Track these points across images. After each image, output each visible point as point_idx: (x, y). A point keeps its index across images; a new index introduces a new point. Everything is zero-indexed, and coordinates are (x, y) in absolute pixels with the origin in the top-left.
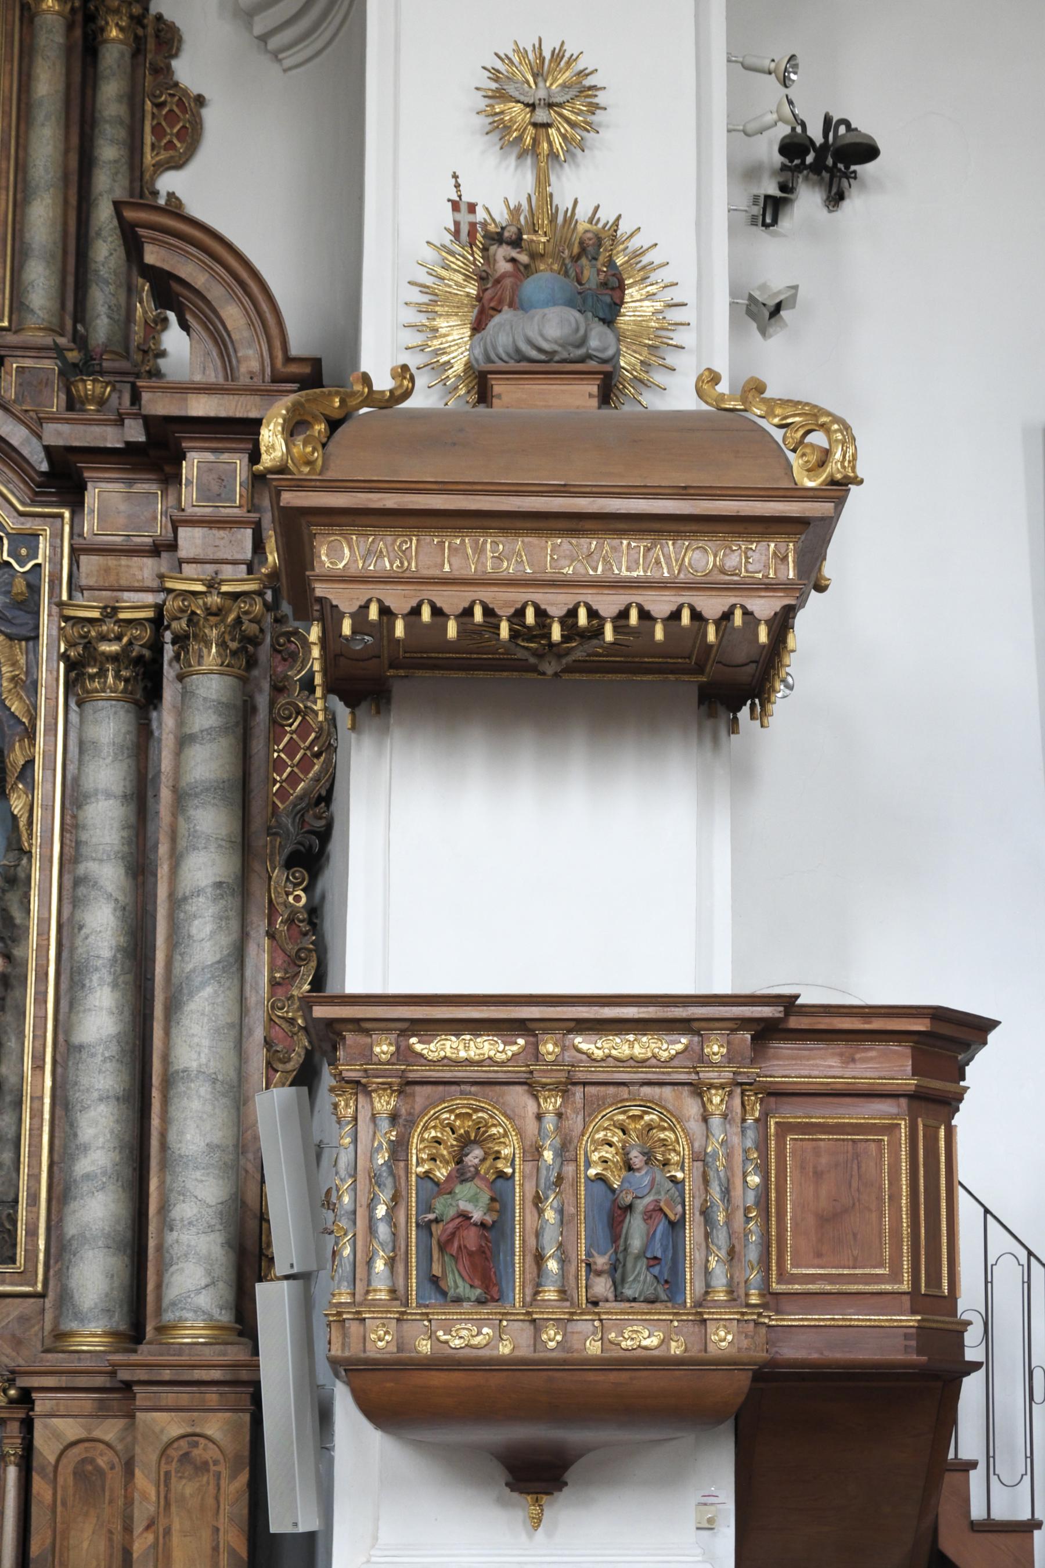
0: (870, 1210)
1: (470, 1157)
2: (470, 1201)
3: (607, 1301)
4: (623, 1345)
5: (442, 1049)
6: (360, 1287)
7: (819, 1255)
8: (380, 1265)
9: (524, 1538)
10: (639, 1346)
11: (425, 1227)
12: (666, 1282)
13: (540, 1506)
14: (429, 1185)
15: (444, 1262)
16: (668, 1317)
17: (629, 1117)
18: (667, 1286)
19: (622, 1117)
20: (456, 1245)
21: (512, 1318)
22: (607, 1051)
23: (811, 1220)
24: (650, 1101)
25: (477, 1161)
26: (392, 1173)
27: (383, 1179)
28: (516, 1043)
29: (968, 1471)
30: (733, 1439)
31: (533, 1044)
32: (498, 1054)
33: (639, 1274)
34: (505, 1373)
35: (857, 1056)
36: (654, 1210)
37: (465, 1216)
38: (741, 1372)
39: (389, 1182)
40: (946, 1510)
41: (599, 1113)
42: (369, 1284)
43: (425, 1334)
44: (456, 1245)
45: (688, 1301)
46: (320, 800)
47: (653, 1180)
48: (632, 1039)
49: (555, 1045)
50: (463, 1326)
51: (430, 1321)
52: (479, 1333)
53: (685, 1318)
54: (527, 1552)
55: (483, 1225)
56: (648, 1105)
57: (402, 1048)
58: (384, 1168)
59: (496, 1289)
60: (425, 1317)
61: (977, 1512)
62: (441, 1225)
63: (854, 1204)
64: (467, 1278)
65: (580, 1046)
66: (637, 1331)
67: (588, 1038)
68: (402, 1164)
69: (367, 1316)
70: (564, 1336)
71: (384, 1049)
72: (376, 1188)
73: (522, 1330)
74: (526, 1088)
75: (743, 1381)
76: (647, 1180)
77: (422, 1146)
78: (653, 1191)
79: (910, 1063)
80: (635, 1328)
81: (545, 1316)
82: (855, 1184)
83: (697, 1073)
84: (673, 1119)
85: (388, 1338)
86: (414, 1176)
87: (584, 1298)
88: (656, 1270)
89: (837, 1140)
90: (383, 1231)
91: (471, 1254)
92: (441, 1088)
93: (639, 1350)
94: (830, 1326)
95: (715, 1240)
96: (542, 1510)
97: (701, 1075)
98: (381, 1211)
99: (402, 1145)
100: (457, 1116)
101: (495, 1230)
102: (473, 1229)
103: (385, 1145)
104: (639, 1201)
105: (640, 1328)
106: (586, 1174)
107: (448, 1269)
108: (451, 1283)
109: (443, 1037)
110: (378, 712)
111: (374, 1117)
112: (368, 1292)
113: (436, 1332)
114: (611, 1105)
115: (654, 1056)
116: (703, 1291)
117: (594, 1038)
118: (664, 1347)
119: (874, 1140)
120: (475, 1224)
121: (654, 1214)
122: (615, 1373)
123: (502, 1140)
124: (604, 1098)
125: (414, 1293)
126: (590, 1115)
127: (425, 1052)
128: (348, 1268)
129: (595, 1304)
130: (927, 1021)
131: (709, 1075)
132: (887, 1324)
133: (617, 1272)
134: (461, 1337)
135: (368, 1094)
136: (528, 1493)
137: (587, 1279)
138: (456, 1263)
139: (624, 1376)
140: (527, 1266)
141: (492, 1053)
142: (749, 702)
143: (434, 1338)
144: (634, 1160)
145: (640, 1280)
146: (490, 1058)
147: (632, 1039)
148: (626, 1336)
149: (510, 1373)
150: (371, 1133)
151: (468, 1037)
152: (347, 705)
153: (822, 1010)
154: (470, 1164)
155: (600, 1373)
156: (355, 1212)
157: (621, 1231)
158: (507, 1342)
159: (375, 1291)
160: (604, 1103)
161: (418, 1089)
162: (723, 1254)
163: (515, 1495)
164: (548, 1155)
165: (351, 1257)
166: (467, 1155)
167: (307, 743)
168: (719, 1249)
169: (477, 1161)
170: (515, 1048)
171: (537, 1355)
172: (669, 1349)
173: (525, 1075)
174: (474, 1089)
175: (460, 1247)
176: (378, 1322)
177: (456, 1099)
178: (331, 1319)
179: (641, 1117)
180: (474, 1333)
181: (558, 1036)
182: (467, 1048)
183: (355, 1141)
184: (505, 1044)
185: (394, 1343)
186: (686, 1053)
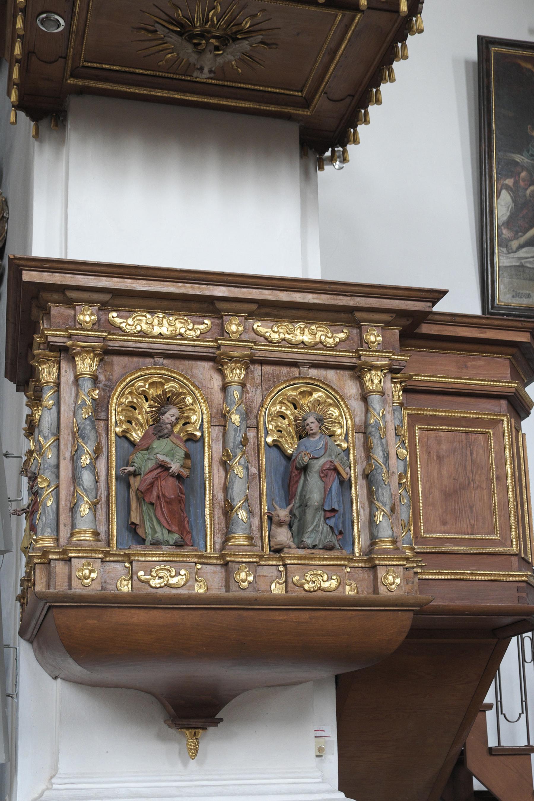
0: (482, 488)
1: (167, 415)
2: (166, 455)
3: (290, 547)
4: (306, 587)
5: (138, 324)
6: (64, 532)
7: (444, 523)
8: (84, 509)
9: (180, 766)
10: (319, 588)
11: (124, 480)
12: (341, 533)
13: (197, 739)
14: (126, 444)
15: (141, 511)
16: (342, 563)
17: (301, 393)
18: (340, 537)
19: (294, 393)
20: (155, 493)
21: (206, 561)
22: (282, 336)
23: (437, 494)
25: (173, 419)
26: (94, 428)
28: (204, 323)
29: (485, 711)
30: (335, 686)
31: (218, 325)
32: (188, 332)
33: (317, 525)
34: (200, 612)
35: (469, 364)
36: (329, 469)
37: (164, 467)
38: (404, 613)
39: (92, 435)
40: (471, 740)
41: (275, 388)
42: (73, 526)
43: (126, 575)
44: (155, 493)
45: (357, 550)
47: (326, 444)
48: (303, 326)
49: (238, 325)
50: (162, 567)
51: (131, 562)
52: (178, 574)
53: (356, 564)
54: (183, 778)
55: (179, 477)
56: (317, 384)
57: (102, 321)
58: (88, 422)
59: (189, 536)
60: (126, 559)
61: (492, 742)
62: (138, 478)
63: (469, 483)
64: (165, 524)
65: (259, 329)
66: (317, 574)
67: (265, 323)
68: (102, 423)
69: (73, 555)
70: (255, 577)
71: (87, 316)
72: (80, 441)
73: (215, 573)
74: (211, 364)
75: (406, 620)
76: (321, 444)
77: (119, 409)
78: (327, 453)
79: (509, 371)
80: (315, 572)
81: (240, 559)
82: (469, 467)
83: (359, 357)
84: (337, 398)
85: (94, 575)
86: (113, 435)
87: (268, 547)
88: (332, 522)
90: (87, 477)
91: (169, 502)
92: (136, 359)
93: (319, 591)
94: (460, 580)
95: (381, 498)
96: (198, 743)
97: (363, 358)
98: (85, 460)
99: (102, 407)
100: (152, 384)
101: (188, 482)
102: (171, 480)
103: (88, 403)
104: (315, 461)
105: (320, 572)
106: (266, 442)
107: (146, 517)
108: (149, 530)
109: (139, 313)
110: (56, 125)
111: (77, 379)
112: (72, 535)
113: (137, 572)
114: (285, 382)
116: (368, 543)
117: (270, 324)
118: (340, 589)
119: (481, 433)
120: (173, 476)
121: (330, 473)
122: (297, 613)
123: (191, 407)
124: (279, 376)
125: (115, 538)
126: (267, 390)
127: (123, 325)
128: (51, 516)
129: (278, 551)
130: (528, 334)
131: (367, 358)
132: (505, 579)
133: (297, 525)
134: (160, 578)
135: (72, 360)
136: (188, 728)
137: (269, 531)
138: (155, 510)
139: (306, 615)
140: (216, 518)
141: (183, 331)
142: (330, 149)
143: (135, 578)
144: (311, 425)
145: (317, 530)
146: (181, 334)
147: (303, 326)
148: (308, 579)
149: (204, 612)
150: (73, 395)
151: (161, 315)
152: (33, 119)
153: (449, 318)
154: (167, 421)
155: (285, 612)
156: (58, 467)
157: (296, 490)
158: (202, 583)
159: (80, 532)
160: (278, 380)
161: (116, 359)
162: (387, 509)
163: (173, 732)
164: (236, 418)
165: (54, 506)
166: (164, 414)
168: (384, 505)
169: (173, 419)
170: (202, 327)
171: (230, 595)
172: (344, 591)
173: (212, 350)
174: (166, 362)
175: (158, 496)
176: (84, 561)
177: (150, 369)
178: (36, 561)
179: (311, 394)
180: (173, 573)
181: (241, 318)
182: (161, 324)
183: (58, 404)
184: (194, 323)
185: (98, 581)
186: (347, 342)
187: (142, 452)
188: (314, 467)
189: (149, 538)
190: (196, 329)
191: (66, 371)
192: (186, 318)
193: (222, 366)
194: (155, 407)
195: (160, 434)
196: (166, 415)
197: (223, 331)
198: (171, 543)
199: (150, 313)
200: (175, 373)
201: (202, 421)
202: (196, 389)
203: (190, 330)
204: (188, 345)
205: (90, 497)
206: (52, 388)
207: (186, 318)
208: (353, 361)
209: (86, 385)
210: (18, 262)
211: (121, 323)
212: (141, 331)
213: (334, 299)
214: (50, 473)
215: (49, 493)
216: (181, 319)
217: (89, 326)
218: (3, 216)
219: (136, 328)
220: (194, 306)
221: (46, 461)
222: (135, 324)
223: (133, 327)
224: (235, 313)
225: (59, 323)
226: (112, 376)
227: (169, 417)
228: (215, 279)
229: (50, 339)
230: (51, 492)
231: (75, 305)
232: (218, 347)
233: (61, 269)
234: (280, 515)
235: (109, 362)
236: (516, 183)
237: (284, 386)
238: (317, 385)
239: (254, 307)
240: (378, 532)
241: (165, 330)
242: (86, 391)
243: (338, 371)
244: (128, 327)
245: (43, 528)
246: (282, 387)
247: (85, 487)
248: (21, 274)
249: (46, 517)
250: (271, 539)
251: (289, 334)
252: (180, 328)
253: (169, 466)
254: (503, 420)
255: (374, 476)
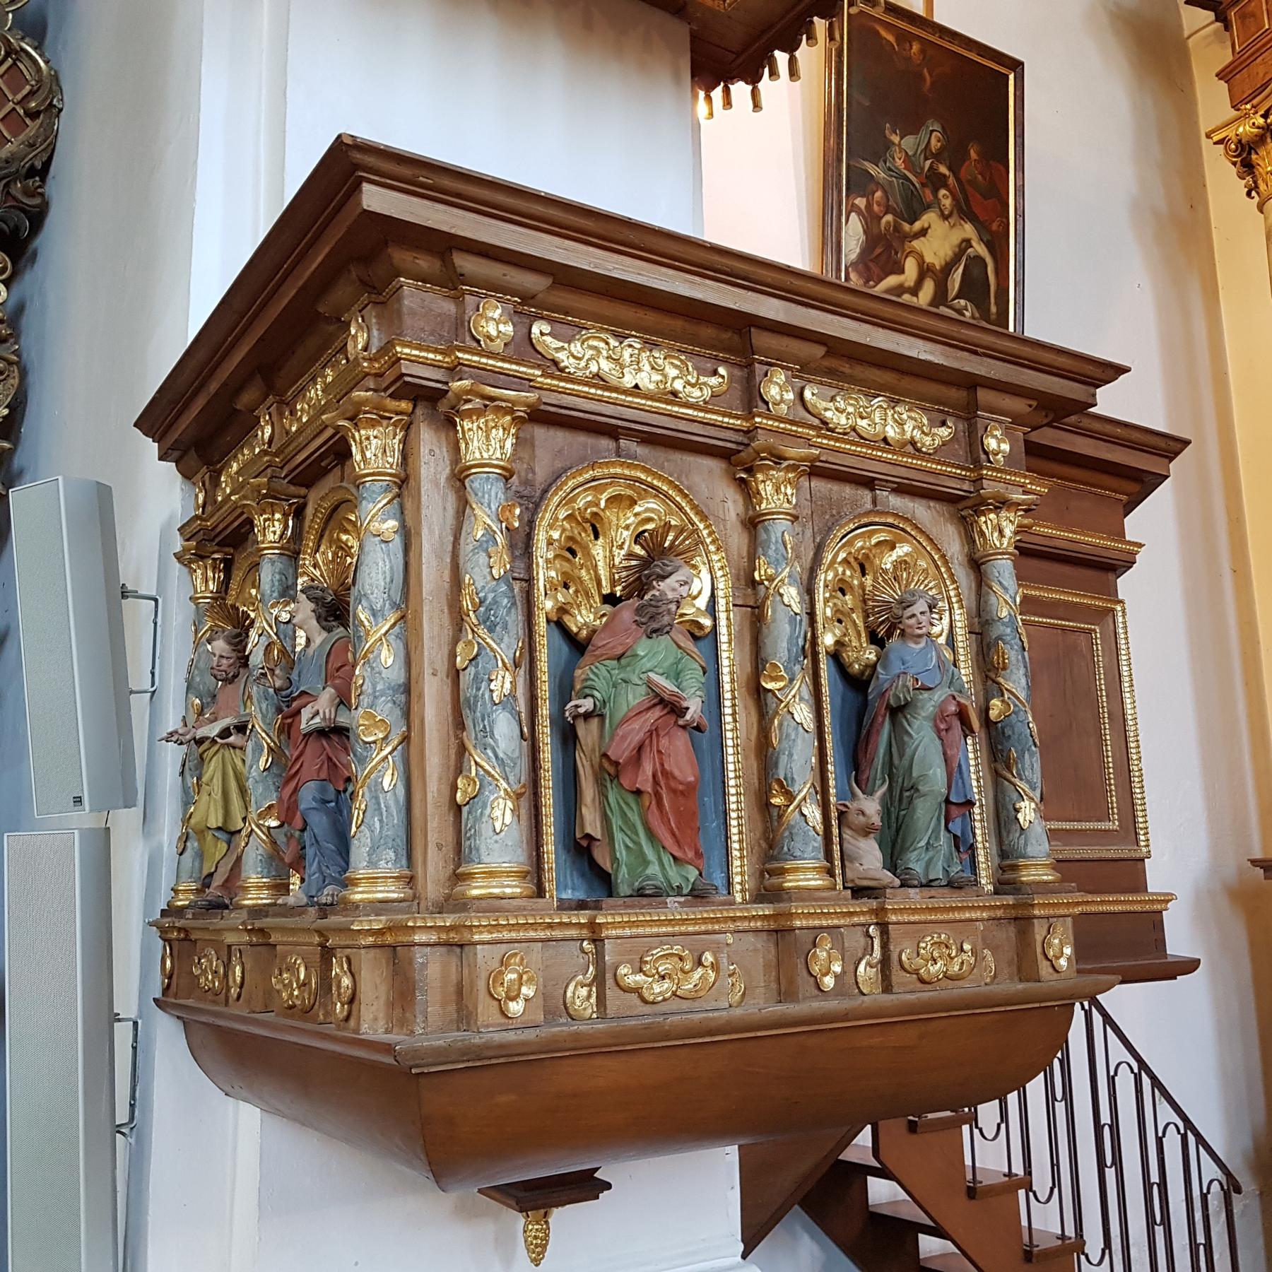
20: (648, 768)
24: (906, 520)
27: (502, 612)
46: (32, 172)
56: (903, 528)
64: (669, 842)
89: (1054, 627)
92: (582, 439)
104: (926, 695)
107: (616, 822)
111: (460, 477)
115: (913, 443)
119: (1083, 631)
127: (561, 356)
141: (678, 385)
146: (674, 393)
154: (670, 595)
165: (401, 791)
167: (19, 97)
170: (714, 381)
187: (607, 662)
188: (922, 708)
189: (623, 878)
190: (704, 384)
191: (431, 450)
192: (683, 358)
193: (750, 471)
194: (637, 557)
195: (655, 626)
196: (668, 581)
197: (752, 398)
198: (685, 891)
199: (616, 335)
200: (660, 477)
201: (713, 596)
202: (701, 521)
203: (693, 386)
204: (692, 421)
205: (511, 778)
206: (387, 489)
207: (683, 358)
208: (965, 488)
209: (493, 493)
210: (358, 156)
211: (557, 350)
212: (597, 375)
213: (956, 358)
214: (390, 705)
215: (386, 757)
216: (674, 357)
217: (498, 346)
218: (51, 105)
219: (587, 367)
220: (708, 332)
221: (380, 673)
222: (586, 357)
223: (583, 364)
224: (779, 360)
225: (423, 330)
226: (534, 473)
227: (677, 585)
228: (769, 280)
229: (405, 367)
230: (390, 753)
231: (463, 293)
232: (750, 433)
233: (459, 196)
234: (868, 812)
235: (526, 440)
236: (869, 206)
237: (852, 526)
238: (903, 530)
239: (819, 351)
240: (1026, 844)
241: (647, 380)
242: (494, 508)
243: (932, 504)
244: (572, 360)
245: (374, 849)
246: (848, 529)
247: (501, 755)
248: (356, 187)
249: (381, 821)
250: (847, 863)
251: (862, 418)
252: (674, 379)
253: (685, 704)
254: (1113, 610)
255: (1012, 727)
